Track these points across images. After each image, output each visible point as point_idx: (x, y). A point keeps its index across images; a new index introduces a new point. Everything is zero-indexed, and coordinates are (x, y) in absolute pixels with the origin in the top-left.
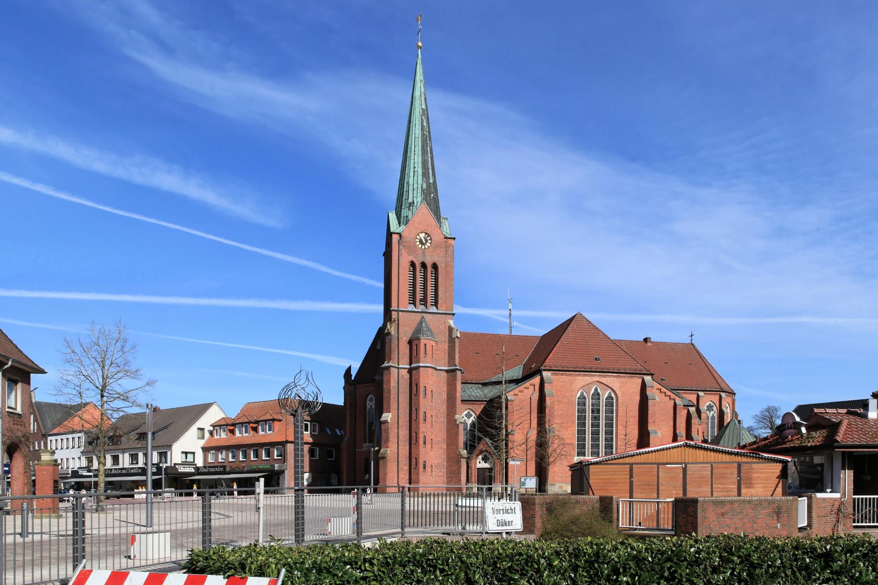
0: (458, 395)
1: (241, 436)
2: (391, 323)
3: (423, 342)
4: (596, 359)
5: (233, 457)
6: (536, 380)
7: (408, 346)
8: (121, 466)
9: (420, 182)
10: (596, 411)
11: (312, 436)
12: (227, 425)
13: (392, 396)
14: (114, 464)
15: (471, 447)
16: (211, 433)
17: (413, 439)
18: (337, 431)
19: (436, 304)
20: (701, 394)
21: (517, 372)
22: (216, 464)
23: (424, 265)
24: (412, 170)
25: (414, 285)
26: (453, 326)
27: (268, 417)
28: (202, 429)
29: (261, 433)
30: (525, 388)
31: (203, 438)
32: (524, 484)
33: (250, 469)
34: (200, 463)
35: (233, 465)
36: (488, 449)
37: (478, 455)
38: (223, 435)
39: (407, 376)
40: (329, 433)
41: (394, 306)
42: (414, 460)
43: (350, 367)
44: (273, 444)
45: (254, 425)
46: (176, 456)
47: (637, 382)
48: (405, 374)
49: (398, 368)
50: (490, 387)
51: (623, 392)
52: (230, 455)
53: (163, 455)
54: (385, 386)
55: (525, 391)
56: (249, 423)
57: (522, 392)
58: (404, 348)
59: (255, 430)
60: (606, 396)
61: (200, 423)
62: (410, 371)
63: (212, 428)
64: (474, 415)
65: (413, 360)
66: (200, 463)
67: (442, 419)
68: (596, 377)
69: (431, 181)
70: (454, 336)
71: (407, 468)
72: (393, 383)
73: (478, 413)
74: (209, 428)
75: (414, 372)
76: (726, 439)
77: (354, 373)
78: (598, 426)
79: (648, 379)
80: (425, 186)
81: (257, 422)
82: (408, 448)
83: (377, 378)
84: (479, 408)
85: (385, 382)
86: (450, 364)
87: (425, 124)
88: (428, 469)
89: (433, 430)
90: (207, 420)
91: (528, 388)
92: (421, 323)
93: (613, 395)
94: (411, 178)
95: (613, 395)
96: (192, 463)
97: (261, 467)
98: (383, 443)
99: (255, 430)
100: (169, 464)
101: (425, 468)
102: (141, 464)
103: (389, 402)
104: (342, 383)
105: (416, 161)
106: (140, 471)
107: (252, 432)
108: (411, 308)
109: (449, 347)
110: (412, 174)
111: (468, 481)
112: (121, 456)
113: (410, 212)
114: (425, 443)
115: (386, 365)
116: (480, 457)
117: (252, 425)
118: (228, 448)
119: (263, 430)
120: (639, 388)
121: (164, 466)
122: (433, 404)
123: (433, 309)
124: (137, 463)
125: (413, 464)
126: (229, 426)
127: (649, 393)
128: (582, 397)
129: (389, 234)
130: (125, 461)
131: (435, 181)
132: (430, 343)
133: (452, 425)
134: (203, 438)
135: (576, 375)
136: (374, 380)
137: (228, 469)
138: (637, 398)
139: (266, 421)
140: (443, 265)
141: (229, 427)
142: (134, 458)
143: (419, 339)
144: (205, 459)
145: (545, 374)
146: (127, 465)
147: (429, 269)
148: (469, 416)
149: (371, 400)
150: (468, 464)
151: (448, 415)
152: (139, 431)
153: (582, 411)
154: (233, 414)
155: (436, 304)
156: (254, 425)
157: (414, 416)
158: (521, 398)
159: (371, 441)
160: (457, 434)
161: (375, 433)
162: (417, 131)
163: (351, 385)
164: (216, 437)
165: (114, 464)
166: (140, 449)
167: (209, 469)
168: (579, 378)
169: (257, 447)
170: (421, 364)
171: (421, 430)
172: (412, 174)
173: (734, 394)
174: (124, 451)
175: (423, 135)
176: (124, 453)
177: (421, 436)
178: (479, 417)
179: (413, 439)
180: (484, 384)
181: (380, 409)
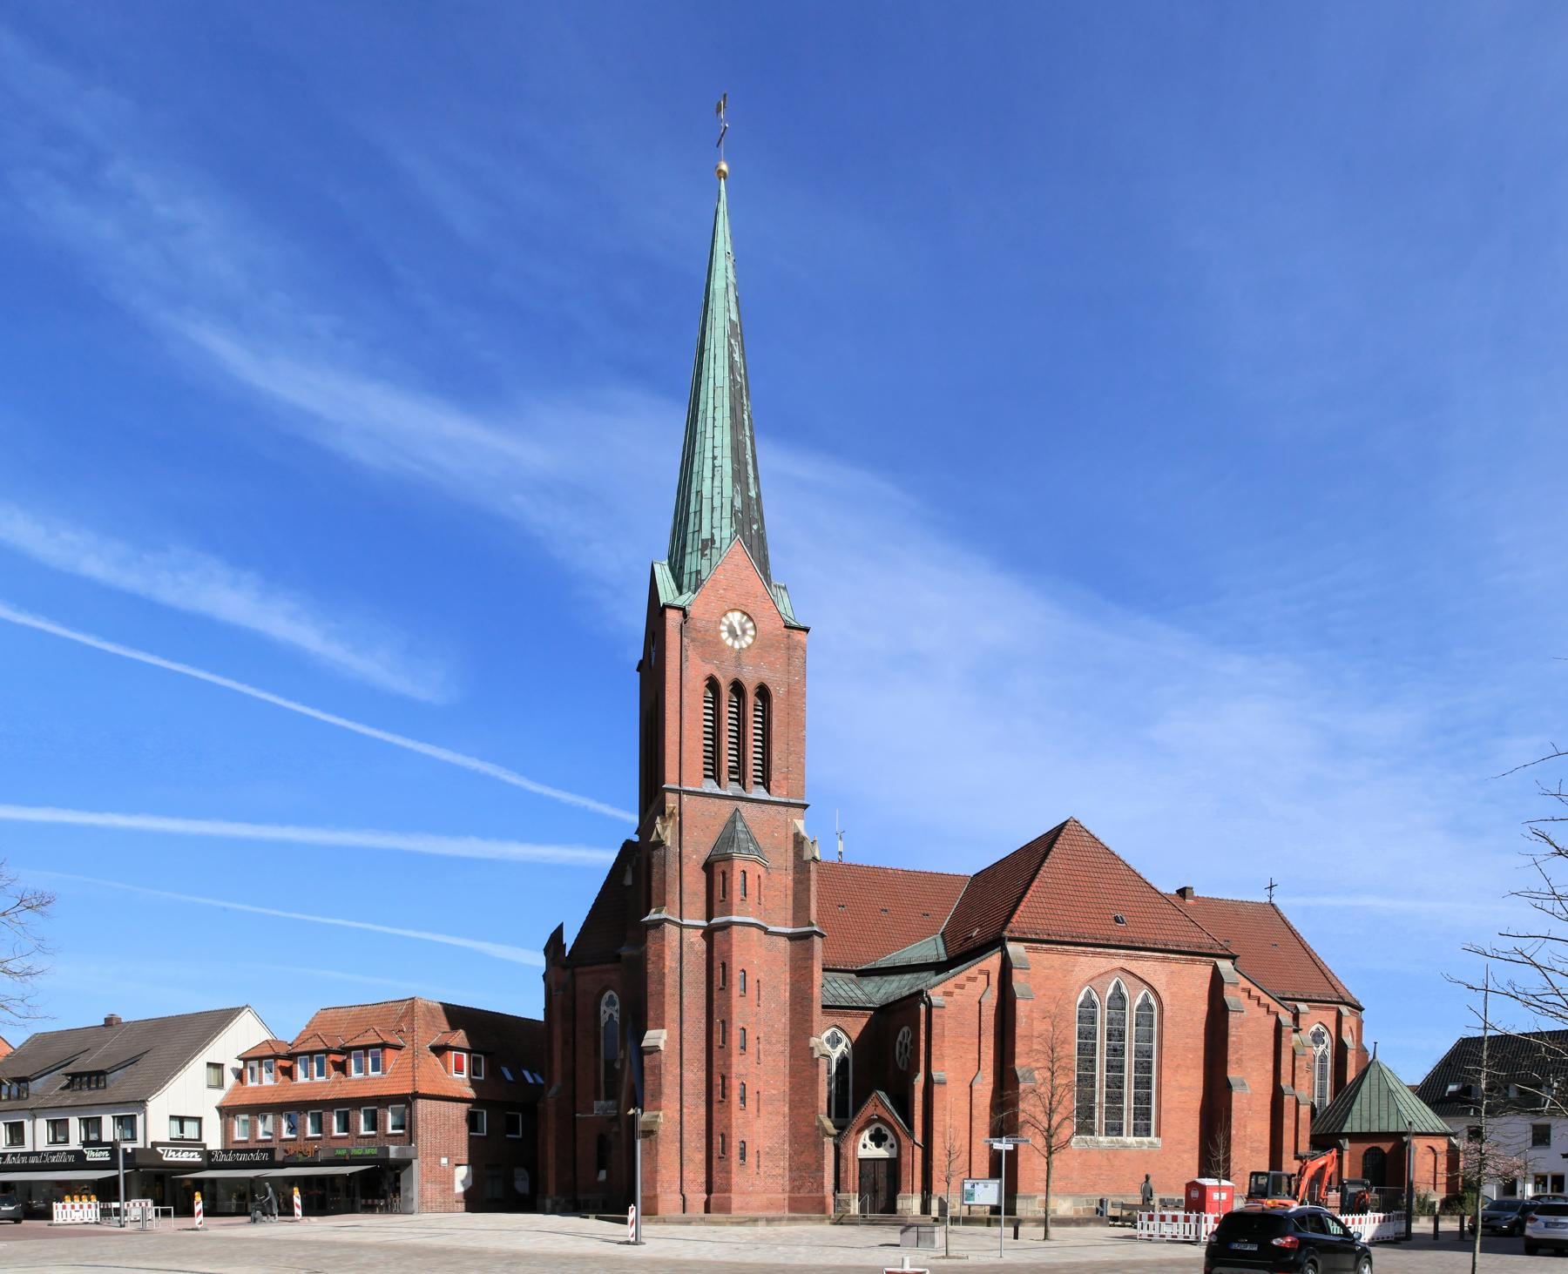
0: (817, 991)
1: (308, 1081)
2: (664, 820)
3: (738, 865)
4: (1116, 920)
5: (292, 1129)
6: (993, 961)
8: (28, 1148)
9: (728, 491)
10: (1116, 1034)
12: (276, 1057)
13: (668, 991)
14: (12, 1143)
15: (844, 1110)
16: (240, 1075)
17: (716, 1091)
19: (765, 782)
20: (1302, 1007)
21: (930, 948)
22: (251, 1146)
23: (738, 688)
24: (708, 462)
25: (715, 734)
26: (803, 833)
27: (371, 1039)
28: (218, 1066)
29: (354, 1075)
30: (970, 979)
31: (220, 1085)
32: (971, 1195)
33: (330, 1155)
34: (213, 1141)
35: (291, 1147)
36: (887, 1116)
37: (860, 1131)
38: (268, 1080)
40: (509, 1077)
41: (671, 781)
42: (717, 1140)
43: (560, 928)
44: (384, 1101)
45: (339, 1058)
46: (156, 1126)
47: (1203, 971)
48: (695, 939)
49: (681, 926)
50: (877, 979)
51: (1174, 996)
52: (285, 1125)
53: (126, 1123)
55: (969, 985)
56: (328, 1052)
57: (961, 987)
58: (695, 881)
59: (342, 1068)
60: (1138, 1001)
61: (212, 1052)
62: (708, 934)
63: (240, 1065)
64: (845, 1040)
65: (716, 908)
66: (213, 1141)
67: (779, 1047)
68: (1119, 960)
69: (753, 494)
70: (807, 856)
71: (701, 1157)
72: (670, 962)
73: (854, 1036)
74: (232, 1063)
75: (718, 935)
76: (1365, 1101)
77: (569, 940)
78: (1121, 1068)
79: (1225, 966)
80: (738, 504)
81: (346, 1051)
82: (703, 1110)
83: (625, 951)
84: (857, 1025)
85: (651, 956)
87: (737, 357)
88: (751, 1159)
89: (761, 1071)
90: (229, 1046)
91: (974, 979)
92: (733, 821)
94: (707, 483)
96: (197, 1143)
97: (357, 1152)
98: (647, 1098)
99: (342, 1068)
100: (139, 1144)
101: (743, 1156)
102: (75, 1144)
103: (662, 1005)
104: (540, 962)
105: (718, 442)
106: (71, 1158)
107: (334, 1074)
108: (710, 786)
109: (796, 882)
110: (708, 473)
111: (837, 1187)
112: (28, 1125)
113: (705, 562)
114: (743, 1099)
115: (653, 916)
116: (866, 1134)
117: (333, 1057)
118: (278, 1109)
119: (359, 1070)
120: (1207, 986)
121: (129, 1147)
122: (760, 1011)
123: (759, 793)
124: (67, 1141)
125: (717, 1149)
126: (282, 1059)
127: (1231, 996)
128: (1089, 1004)
129: (657, 613)
130: (38, 1136)
131: (759, 495)
132: (754, 870)
133: (802, 1058)
134: (220, 1085)
135: (1078, 954)
136: (618, 958)
137: (279, 1157)
138: (1203, 1008)
139: (366, 1048)
141: (281, 1062)
142: (59, 1128)
143: (729, 859)
144: (227, 1132)
145: (1013, 948)
146: (42, 1145)
147: (751, 699)
148: (835, 1041)
149: (611, 1003)
151: (792, 1038)
152: (70, 1069)
153: (1087, 1035)
154: (290, 1032)
155: (765, 782)
156: (339, 1057)
157: (717, 1037)
158: (961, 1000)
159: (612, 1094)
160: (814, 1081)
161: (630, 1078)
162: (719, 371)
163: (565, 967)
164: (250, 1084)
165: (12, 1143)
166: (73, 1109)
167: (234, 1155)
168: (1082, 959)
169: (345, 1107)
170: (735, 918)
171: (734, 1070)
172: (708, 473)
173: (1361, 1009)
174: (34, 1114)
175: (733, 382)
176: (34, 1117)
177: (735, 1084)
178: (857, 1046)
179: (716, 1091)
180: (862, 974)
181: (637, 1017)
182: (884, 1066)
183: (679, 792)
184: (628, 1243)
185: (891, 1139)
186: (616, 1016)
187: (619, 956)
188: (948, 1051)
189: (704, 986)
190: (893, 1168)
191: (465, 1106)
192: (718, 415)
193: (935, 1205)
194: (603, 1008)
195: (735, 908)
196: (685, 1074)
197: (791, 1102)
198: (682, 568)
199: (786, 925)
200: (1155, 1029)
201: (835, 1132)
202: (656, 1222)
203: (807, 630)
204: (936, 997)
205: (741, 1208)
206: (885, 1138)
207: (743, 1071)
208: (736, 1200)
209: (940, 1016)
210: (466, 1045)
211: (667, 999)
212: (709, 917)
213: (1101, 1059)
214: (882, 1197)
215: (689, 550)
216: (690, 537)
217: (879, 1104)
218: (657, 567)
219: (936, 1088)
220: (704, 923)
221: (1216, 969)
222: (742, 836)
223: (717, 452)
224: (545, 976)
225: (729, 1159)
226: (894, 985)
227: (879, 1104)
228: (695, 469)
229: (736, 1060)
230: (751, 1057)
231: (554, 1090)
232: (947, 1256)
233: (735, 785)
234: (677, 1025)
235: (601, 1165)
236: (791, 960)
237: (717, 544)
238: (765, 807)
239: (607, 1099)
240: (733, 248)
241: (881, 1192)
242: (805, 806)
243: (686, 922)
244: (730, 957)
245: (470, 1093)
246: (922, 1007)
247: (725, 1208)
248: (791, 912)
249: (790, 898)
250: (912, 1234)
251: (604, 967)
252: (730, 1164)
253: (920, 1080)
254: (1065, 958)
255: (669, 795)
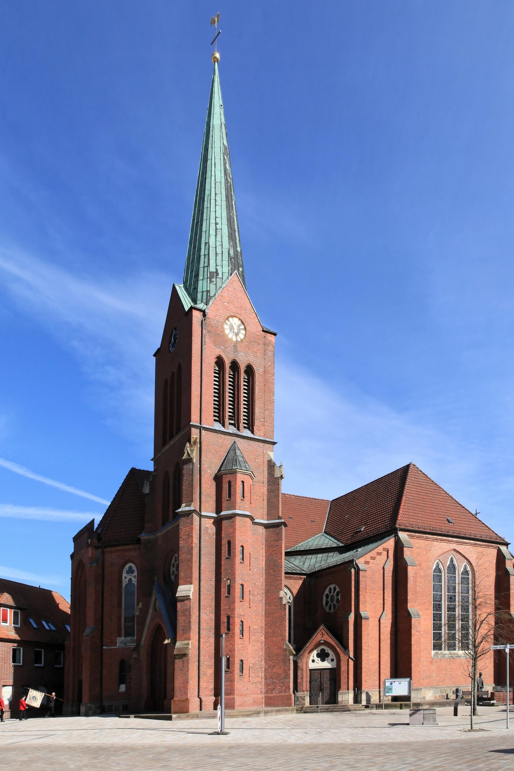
3: (240, 477)
6: (390, 543)
7: (214, 484)
11: (17, 630)
15: (300, 640)
17: (223, 625)
18: (44, 623)
19: (250, 426)
23: (235, 365)
24: (213, 226)
26: (274, 460)
39: (212, 530)
40: (35, 626)
43: (93, 520)
48: (209, 526)
54: (182, 543)
55: (378, 557)
57: (373, 558)
58: (209, 488)
62: (218, 522)
65: (224, 504)
73: (295, 592)
75: (225, 523)
80: (232, 253)
83: (143, 537)
84: (296, 585)
86: (270, 516)
89: (250, 612)
91: (379, 554)
93: (469, 568)
95: (469, 568)
101: (242, 671)
105: (218, 214)
108: (218, 426)
109: (269, 491)
110: (212, 232)
111: (296, 689)
115: (184, 508)
116: (315, 652)
120: (495, 561)
122: (250, 573)
123: (247, 433)
128: (438, 570)
135: (433, 540)
140: (261, 370)
145: (401, 534)
147: (243, 376)
149: (130, 571)
150: (295, 663)
151: (267, 591)
162: (218, 173)
168: (435, 543)
170: (238, 512)
177: (237, 621)
182: (320, 610)
183: (200, 428)
184: (218, 734)
185: (332, 655)
186: (134, 581)
187: (139, 540)
188: (368, 599)
189: (214, 557)
190: (334, 675)
191: (11, 646)
192: (218, 198)
193: (364, 697)
194: (124, 575)
195: (238, 505)
196: (202, 615)
197: (266, 634)
198: (196, 289)
199: (263, 519)
200: (470, 585)
201: (294, 653)
202: (188, 717)
203: (275, 335)
204: (360, 563)
205: (241, 705)
206: (327, 655)
207: (242, 613)
208: (238, 700)
209: (364, 576)
210: (11, 603)
211: (194, 564)
212: (218, 510)
213: (444, 604)
214: (327, 692)
215: (201, 278)
216: (201, 270)
217: (322, 635)
218: (177, 287)
219: (364, 622)
220: (215, 515)
221: (499, 552)
222: (241, 459)
223: (218, 220)
224: (72, 557)
225: (232, 672)
226: (313, 561)
227: (322, 635)
228: (204, 229)
229: (238, 605)
230: (246, 604)
231: (88, 631)
232: (471, 730)
233: (232, 427)
234: (197, 582)
235: (122, 680)
236: (266, 541)
237: (220, 276)
238: (251, 442)
239: (126, 635)
240: (223, 102)
241: (326, 692)
242: (274, 443)
243: (203, 513)
244: (234, 537)
245: (13, 635)
246: (353, 570)
247: (230, 705)
248: (266, 510)
249: (266, 501)
250: (419, 716)
251: (127, 547)
252: (233, 676)
253: (352, 617)
254: (427, 542)
255: (193, 430)
